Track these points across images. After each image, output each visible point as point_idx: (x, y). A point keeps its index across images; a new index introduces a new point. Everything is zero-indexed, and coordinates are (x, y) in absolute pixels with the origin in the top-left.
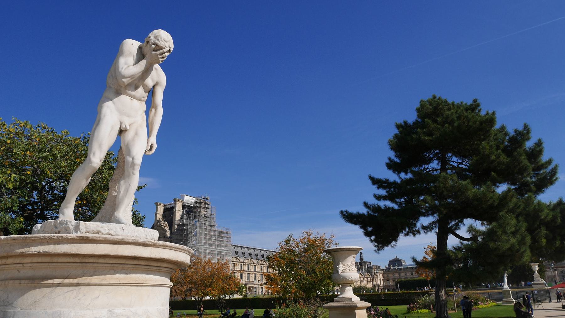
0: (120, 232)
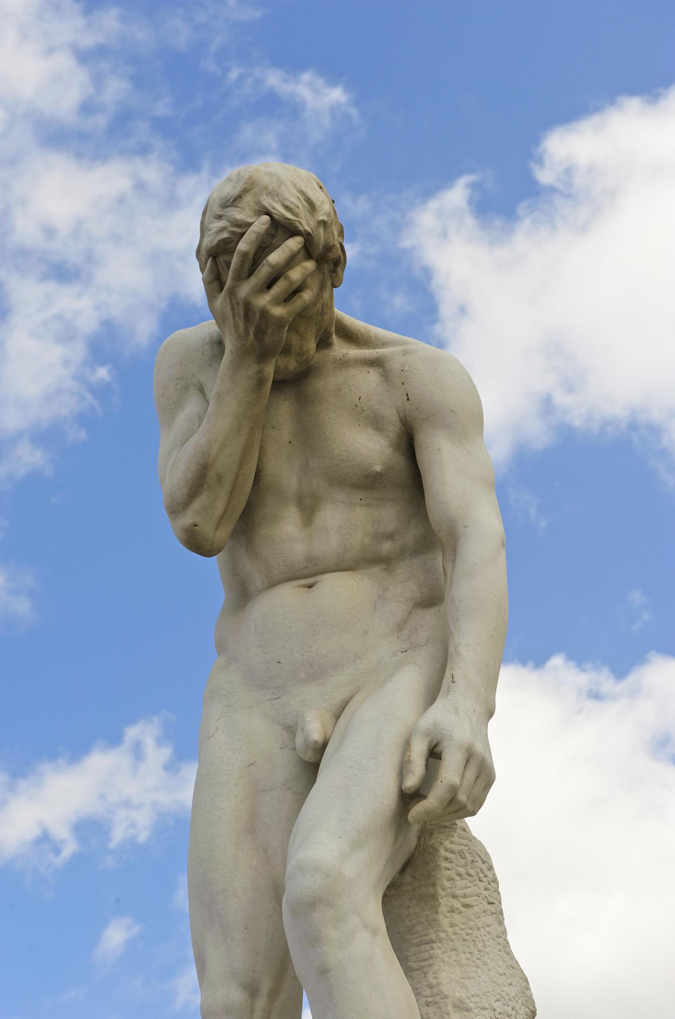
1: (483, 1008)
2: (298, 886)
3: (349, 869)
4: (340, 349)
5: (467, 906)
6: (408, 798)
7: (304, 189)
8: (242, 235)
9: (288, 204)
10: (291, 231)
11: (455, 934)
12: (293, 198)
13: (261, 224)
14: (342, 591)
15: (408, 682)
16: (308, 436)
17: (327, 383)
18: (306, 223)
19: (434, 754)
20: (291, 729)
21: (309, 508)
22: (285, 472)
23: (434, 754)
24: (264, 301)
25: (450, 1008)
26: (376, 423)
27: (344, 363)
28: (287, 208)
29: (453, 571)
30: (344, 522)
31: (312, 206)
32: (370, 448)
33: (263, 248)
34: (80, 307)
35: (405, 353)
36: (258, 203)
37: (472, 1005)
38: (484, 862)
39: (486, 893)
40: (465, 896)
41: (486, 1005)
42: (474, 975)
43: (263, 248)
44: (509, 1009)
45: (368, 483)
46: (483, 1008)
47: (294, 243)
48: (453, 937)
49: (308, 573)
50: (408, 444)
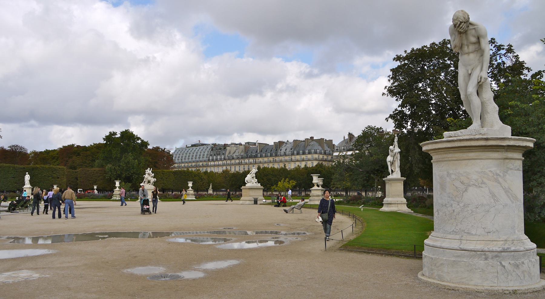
2: (468, 93)
4: (471, 27)
6: (478, 83)
14: (472, 56)
15: (478, 69)
16: (467, 39)
17: (469, 32)
19: (481, 78)
20: (468, 71)
21: (468, 46)
22: (465, 42)
23: (481, 78)
24: (460, 30)
26: (474, 36)
27: (471, 29)
30: (472, 48)
32: (473, 39)
33: (460, 25)
43: (460, 25)
45: (474, 43)
47: (463, 23)
49: (468, 53)
50: (478, 38)
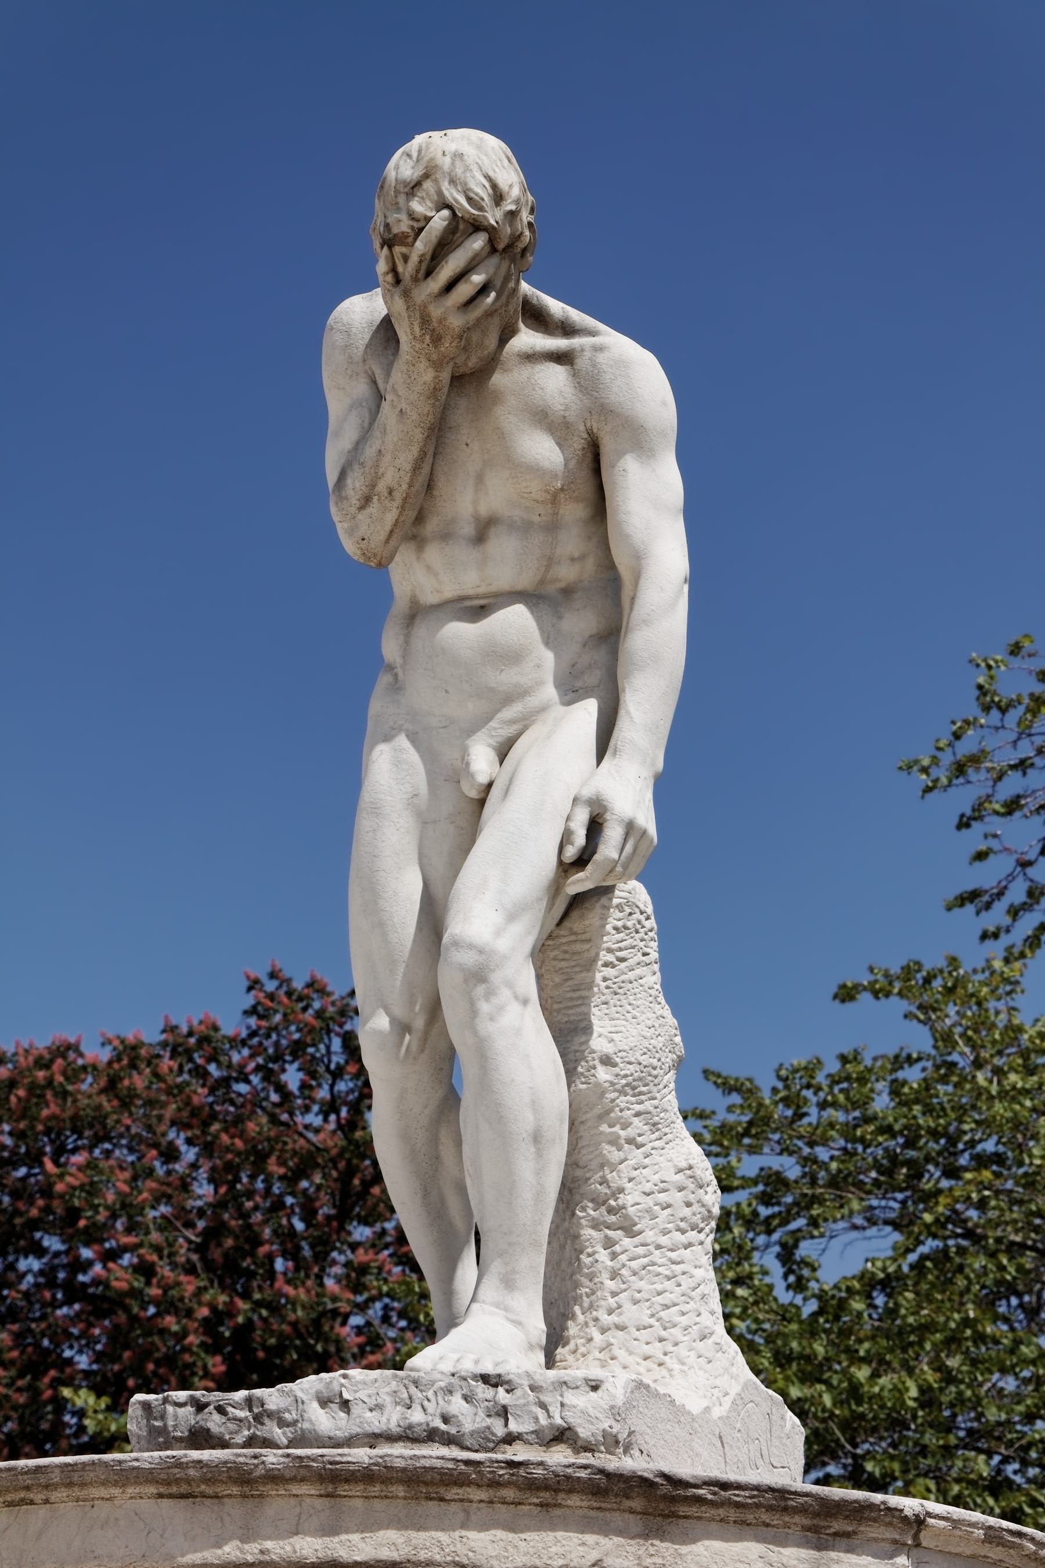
0: (324, 1421)
1: (630, 1063)
3: (502, 945)
5: (622, 960)
7: (491, 174)
8: (421, 230)
9: (472, 195)
10: (477, 226)
11: (607, 987)
12: (483, 192)
13: (440, 220)
18: (493, 216)
19: (595, 827)
23: (595, 827)
25: (597, 1062)
26: (556, 426)
28: (469, 199)
29: (631, 609)
31: (498, 197)
34: (571, 1346)
35: (599, 349)
36: (440, 193)
37: (618, 1060)
38: (642, 913)
39: (642, 944)
40: (620, 949)
41: (633, 1060)
42: (622, 1029)
44: (655, 1062)
46: (630, 1063)
47: (478, 243)
48: (606, 991)
